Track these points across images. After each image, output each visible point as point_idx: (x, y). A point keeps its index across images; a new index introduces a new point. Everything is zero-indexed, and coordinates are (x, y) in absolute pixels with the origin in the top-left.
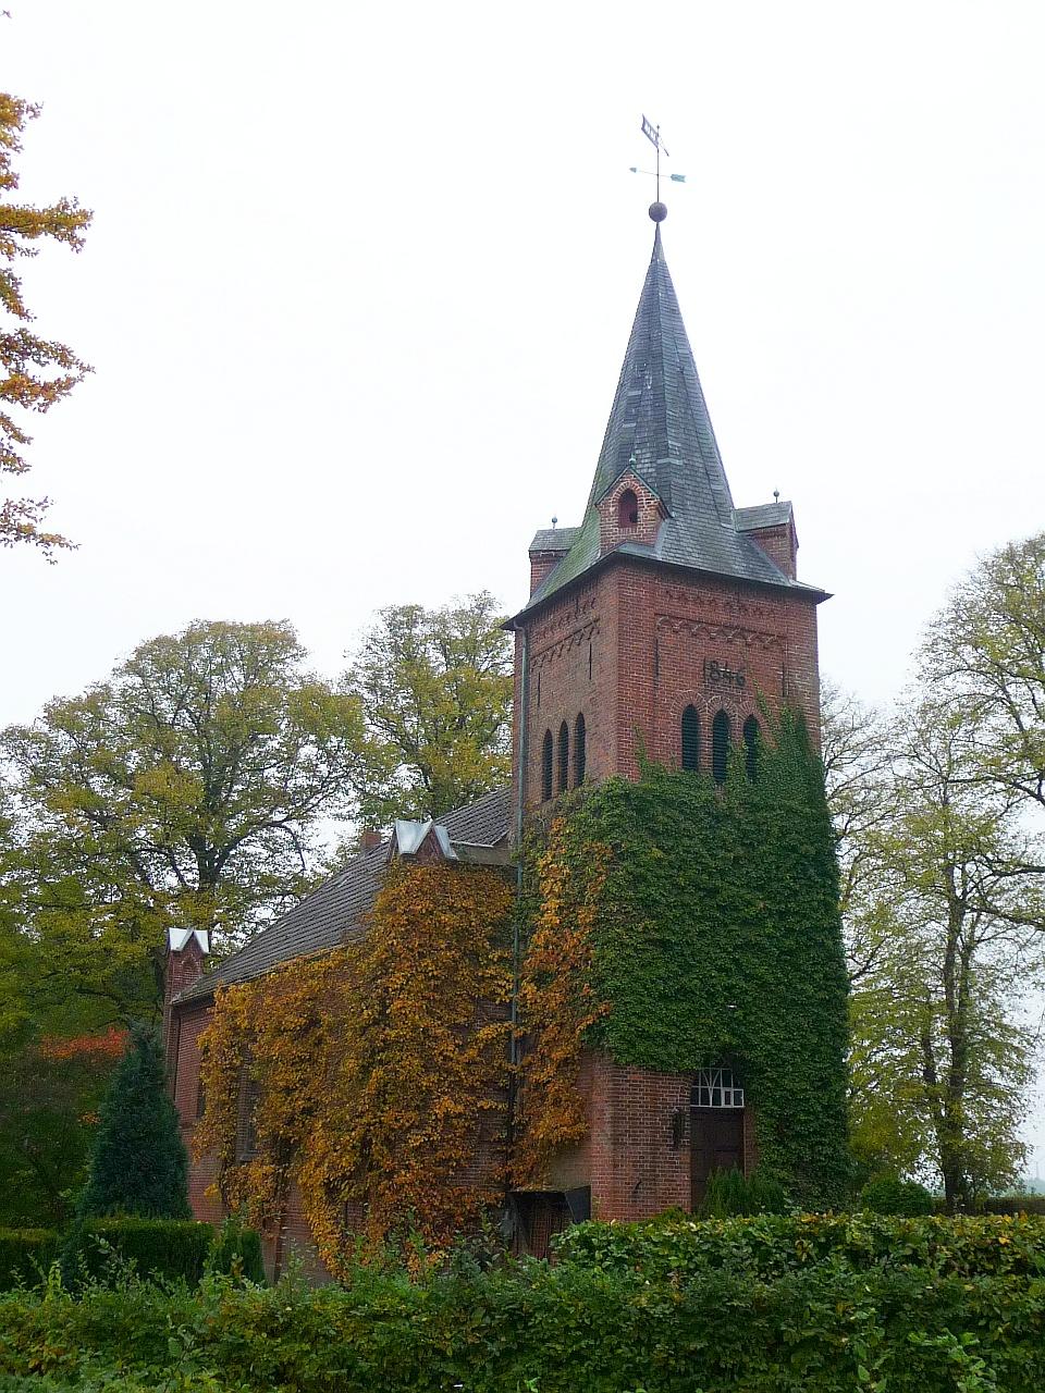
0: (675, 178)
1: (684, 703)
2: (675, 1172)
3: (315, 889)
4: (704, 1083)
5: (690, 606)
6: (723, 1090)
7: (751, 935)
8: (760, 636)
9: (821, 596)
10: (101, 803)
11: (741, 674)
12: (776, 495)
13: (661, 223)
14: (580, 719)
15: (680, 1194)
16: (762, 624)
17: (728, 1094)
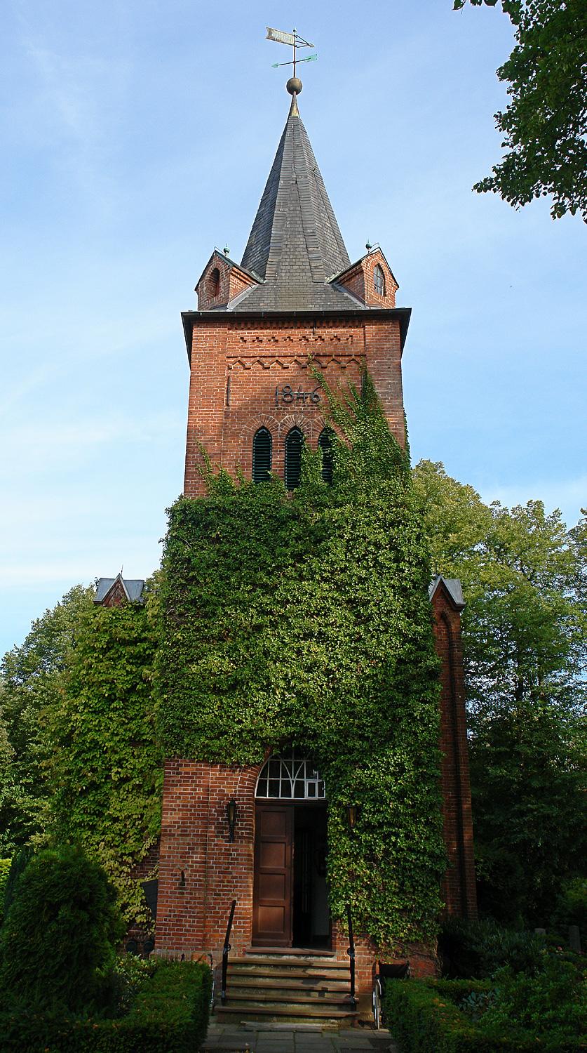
1: (257, 425)
2: (231, 864)
4: (285, 775)
6: (307, 782)
7: (315, 625)
10: (320, 543)
15: (237, 886)
17: (312, 786)
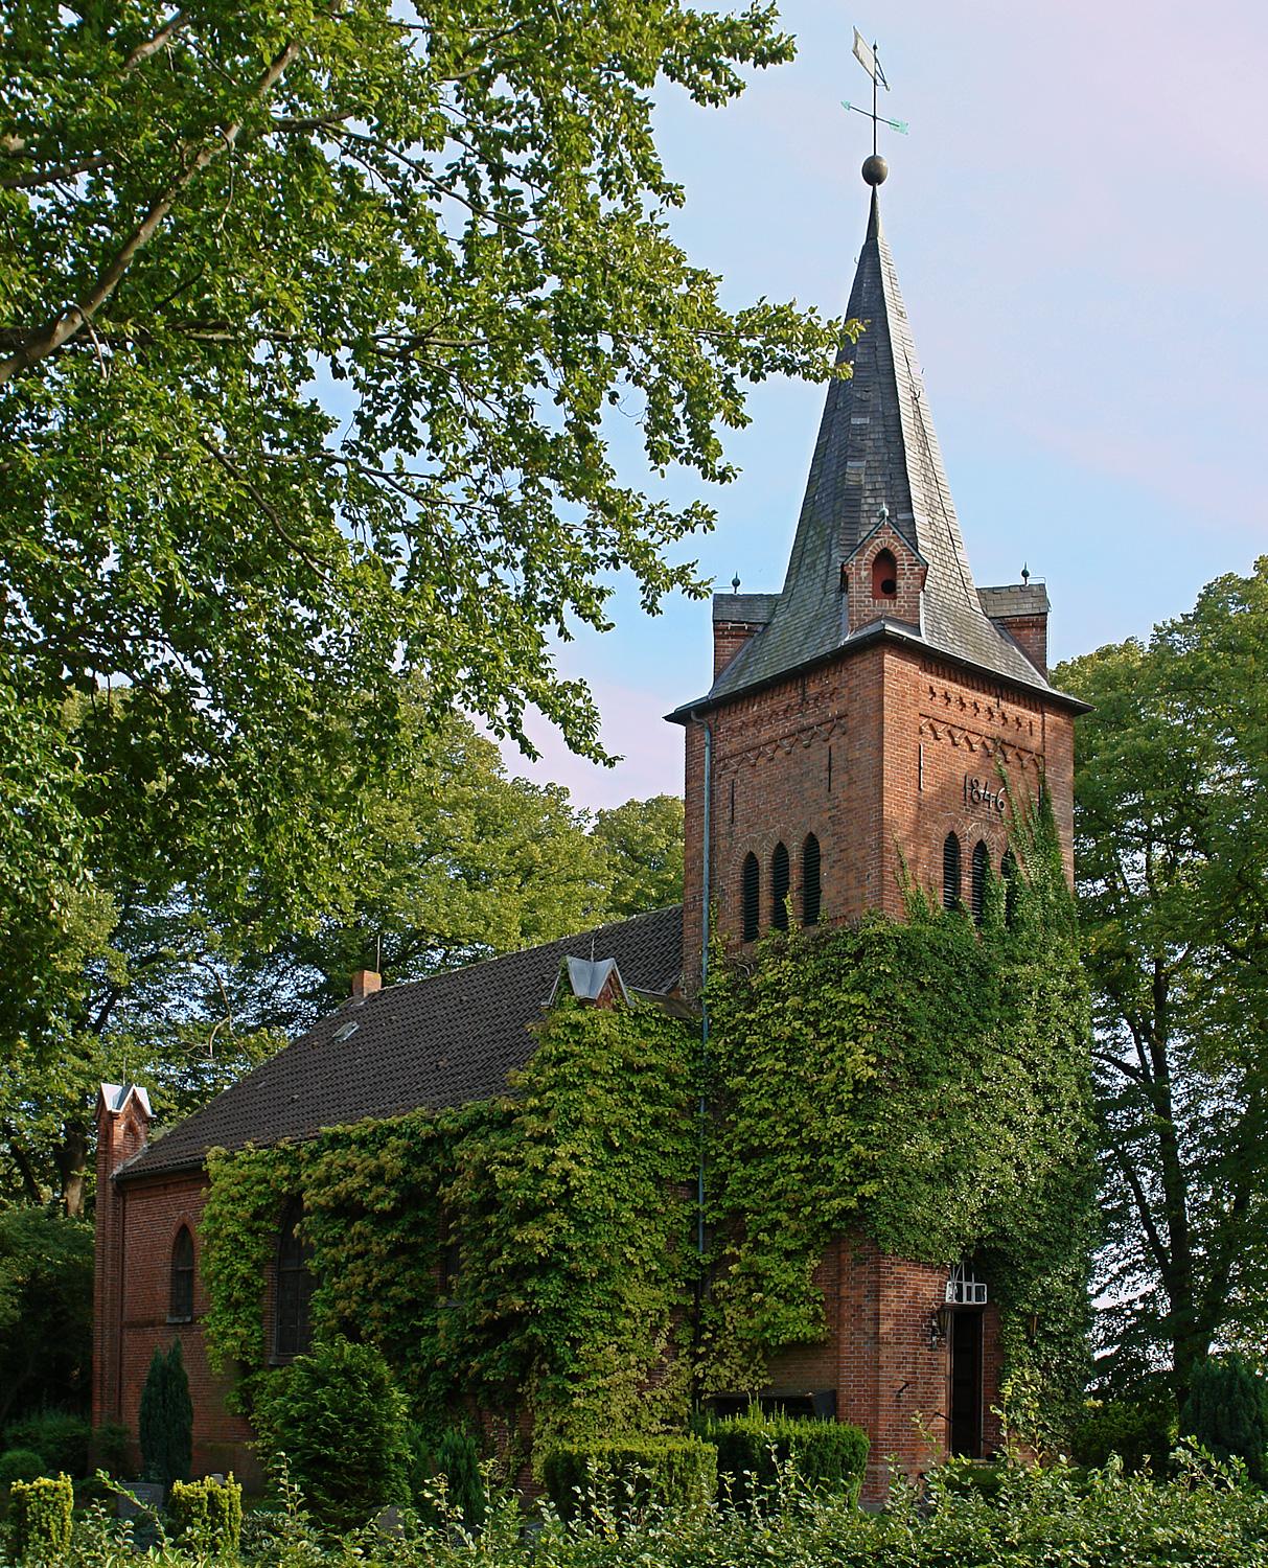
3: (438, 1057)
6: (965, 1285)
12: (1025, 574)
14: (811, 844)
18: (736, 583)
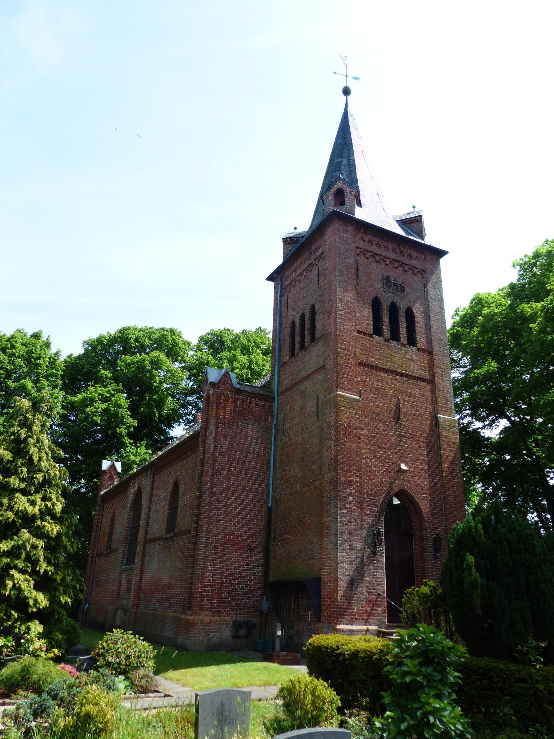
0: (355, 78)
5: (374, 246)
8: (413, 268)
9: (440, 253)
11: (403, 285)
12: (414, 207)
13: (348, 97)
16: (414, 262)
18: (295, 228)
